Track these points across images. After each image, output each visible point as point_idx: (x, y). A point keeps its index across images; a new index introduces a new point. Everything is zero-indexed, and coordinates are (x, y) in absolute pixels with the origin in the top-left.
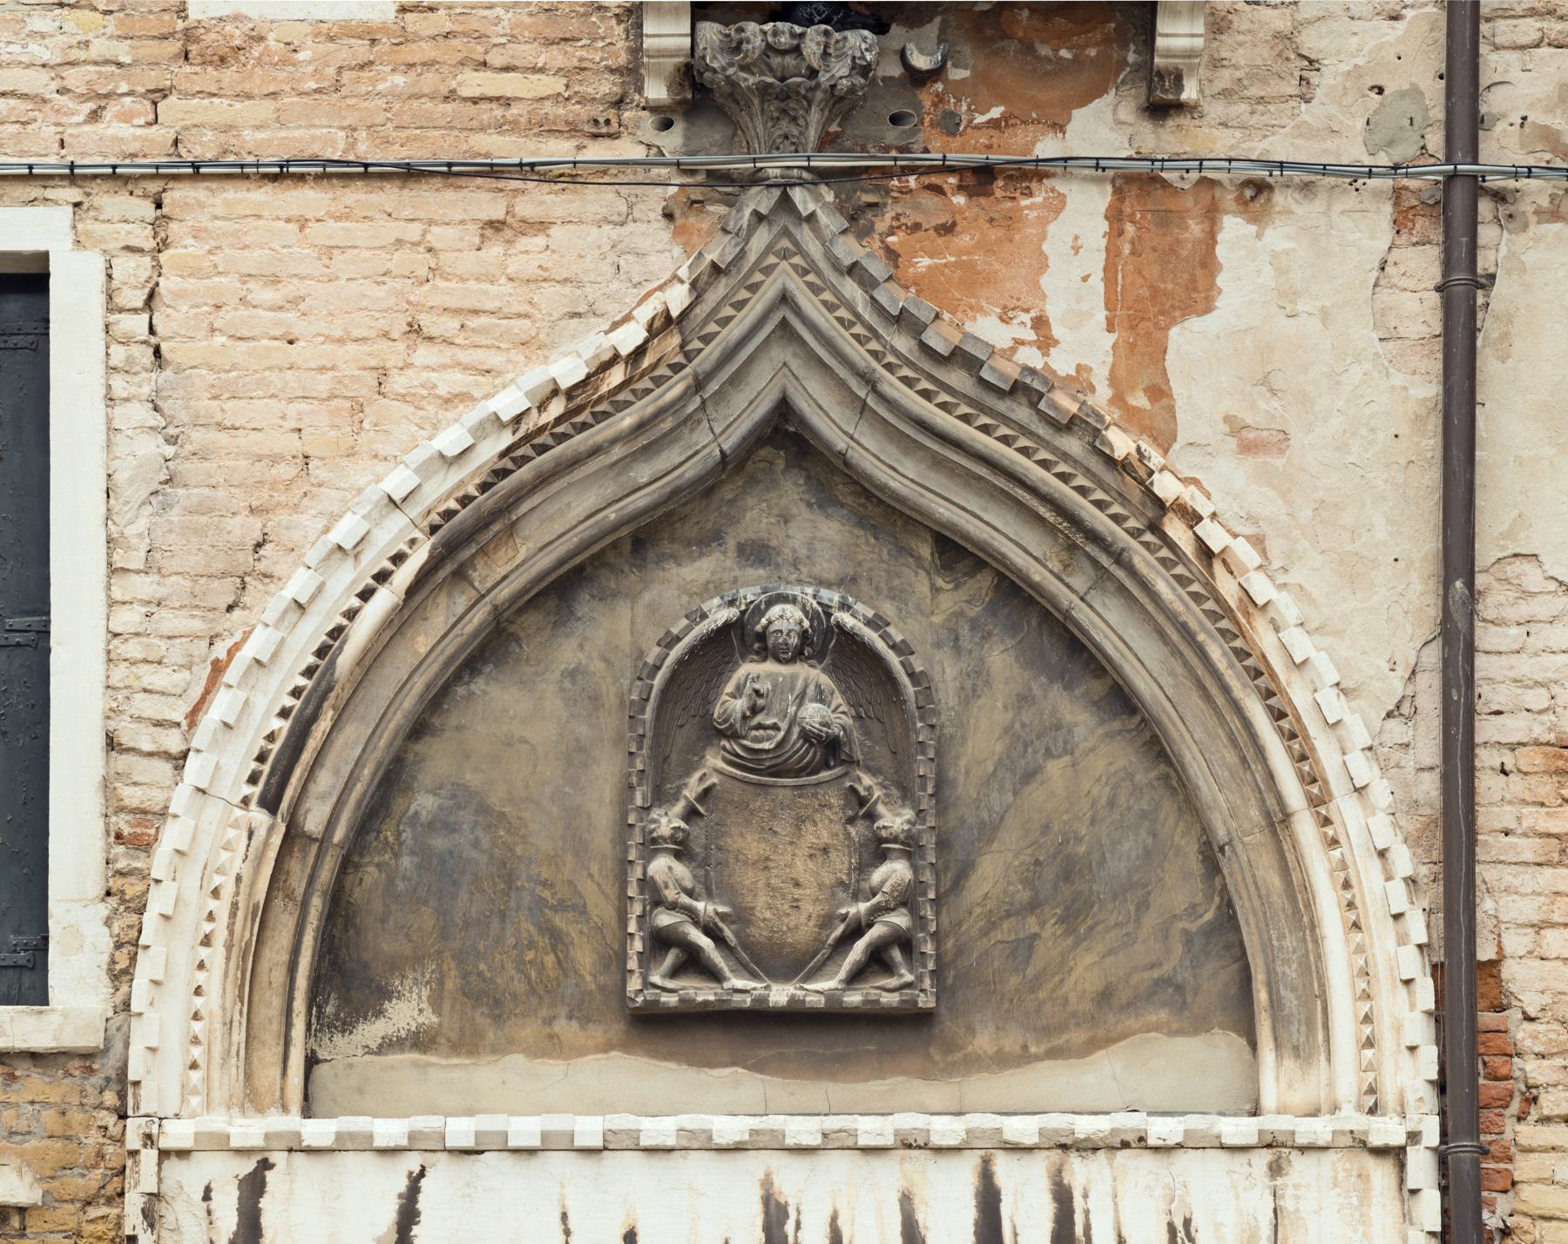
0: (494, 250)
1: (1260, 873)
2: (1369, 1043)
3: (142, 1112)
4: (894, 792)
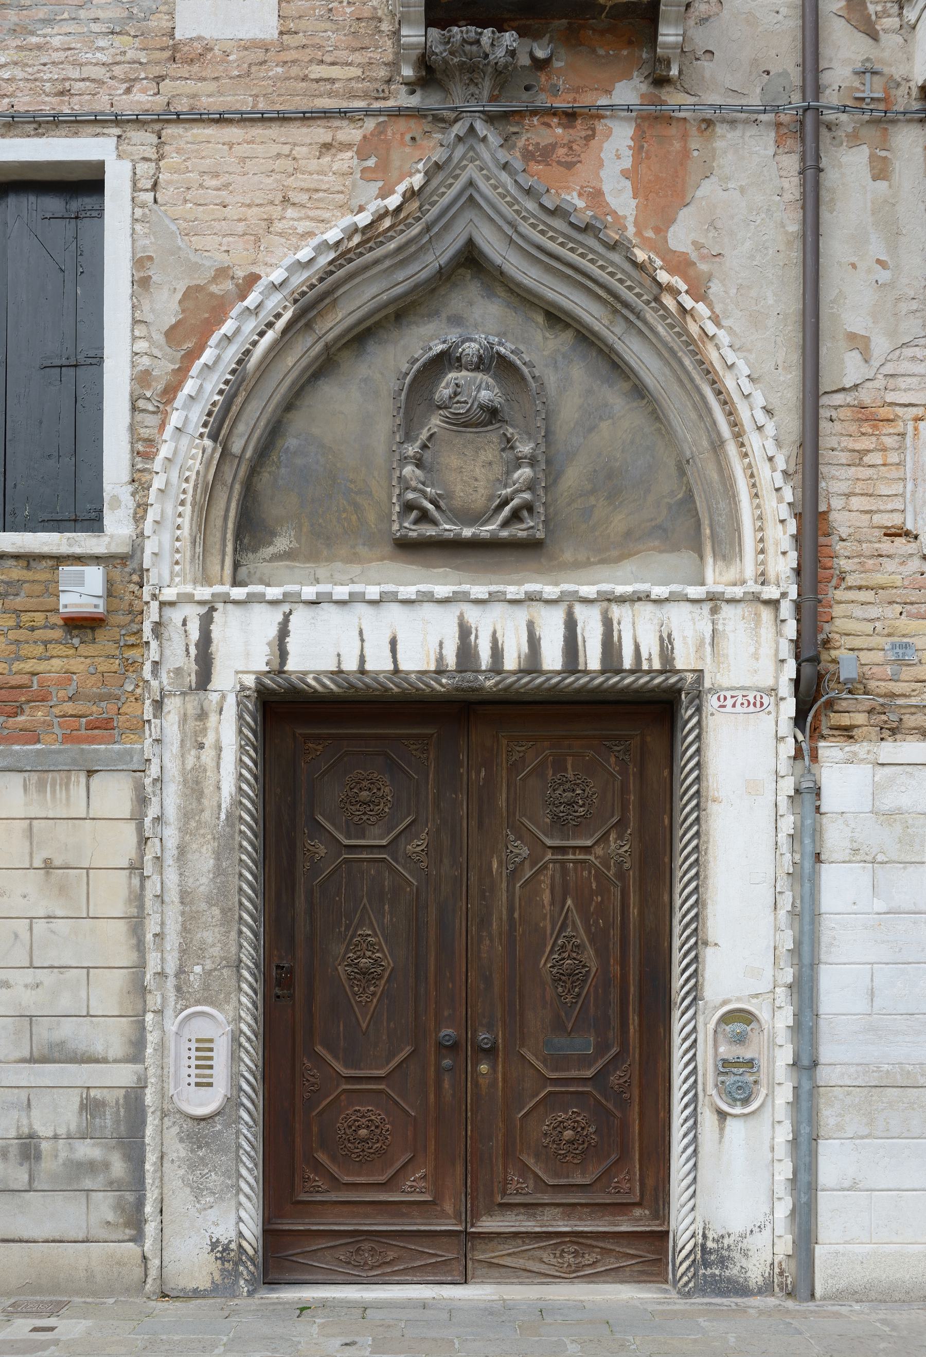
0: (326, 159)
2: (762, 551)
4: (525, 436)
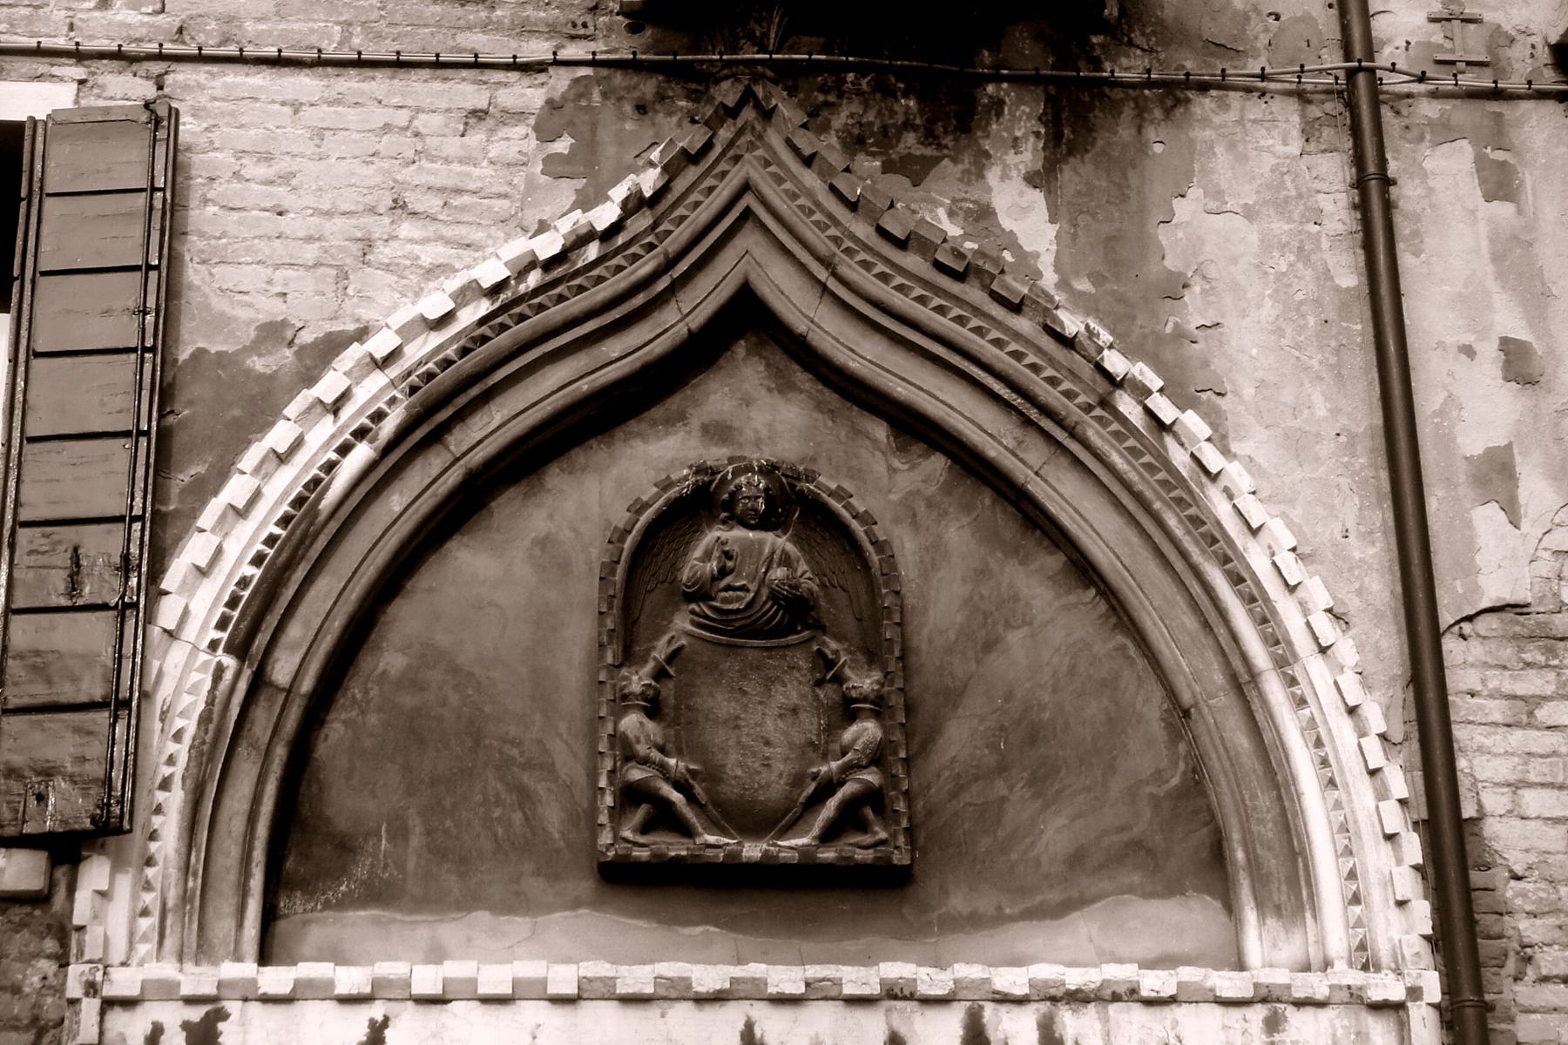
0: (477, 137)
1: (1227, 735)
2: (1356, 899)
3: (86, 957)
4: (860, 657)
